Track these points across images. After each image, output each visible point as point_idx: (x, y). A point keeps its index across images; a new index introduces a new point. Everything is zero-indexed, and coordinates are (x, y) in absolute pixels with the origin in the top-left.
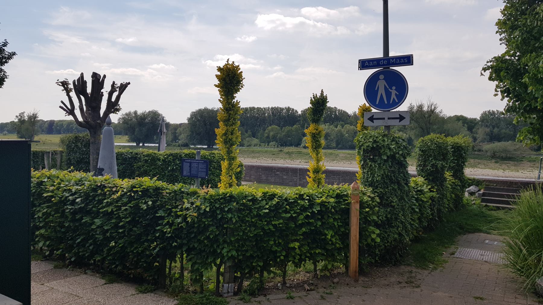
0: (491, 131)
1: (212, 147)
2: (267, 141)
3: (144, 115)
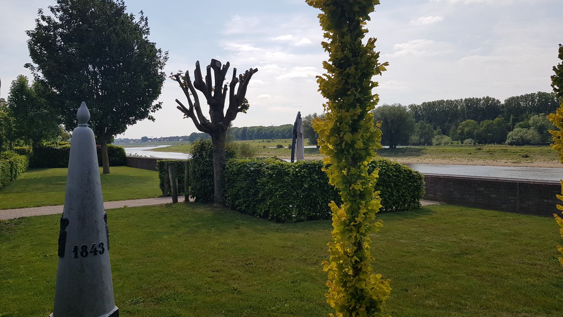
1: (395, 147)
2: (462, 137)
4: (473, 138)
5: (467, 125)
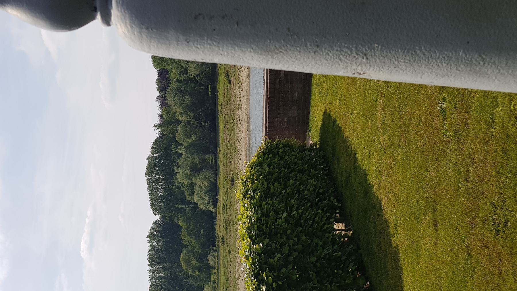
2: (206, 269)
4: (207, 253)
5: (188, 262)
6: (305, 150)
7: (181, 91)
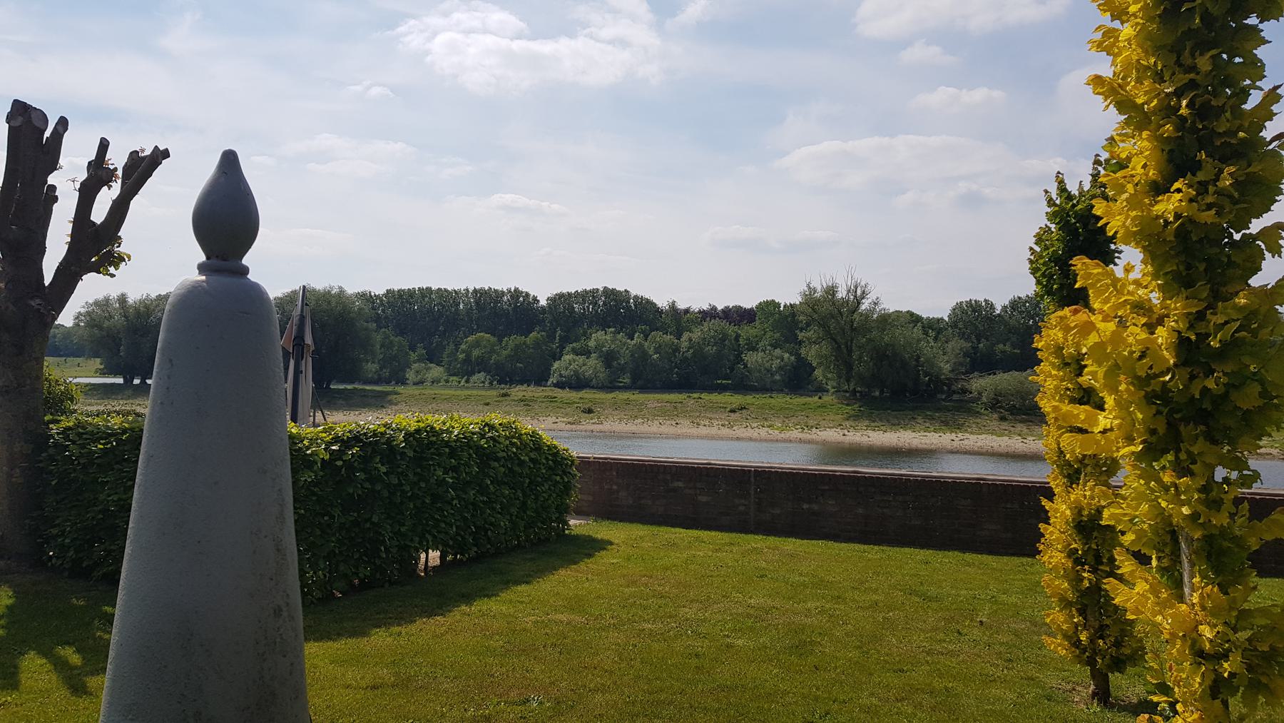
0: (973, 348)
2: (466, 369)
3: (146, 307)
4: (488, 372)
5: (477, 344)
6: (561, 513)
7: (723, 340)
